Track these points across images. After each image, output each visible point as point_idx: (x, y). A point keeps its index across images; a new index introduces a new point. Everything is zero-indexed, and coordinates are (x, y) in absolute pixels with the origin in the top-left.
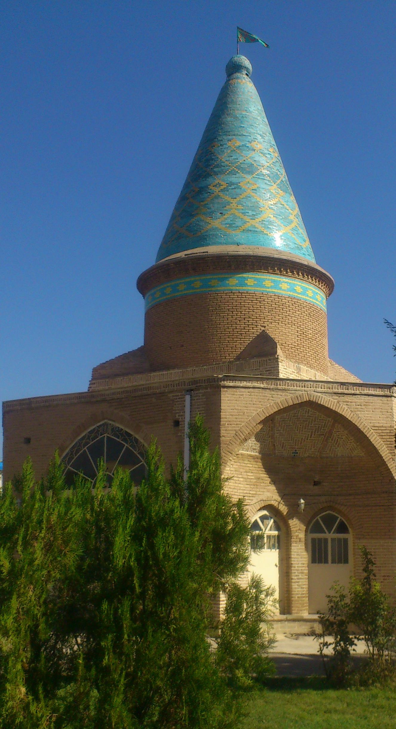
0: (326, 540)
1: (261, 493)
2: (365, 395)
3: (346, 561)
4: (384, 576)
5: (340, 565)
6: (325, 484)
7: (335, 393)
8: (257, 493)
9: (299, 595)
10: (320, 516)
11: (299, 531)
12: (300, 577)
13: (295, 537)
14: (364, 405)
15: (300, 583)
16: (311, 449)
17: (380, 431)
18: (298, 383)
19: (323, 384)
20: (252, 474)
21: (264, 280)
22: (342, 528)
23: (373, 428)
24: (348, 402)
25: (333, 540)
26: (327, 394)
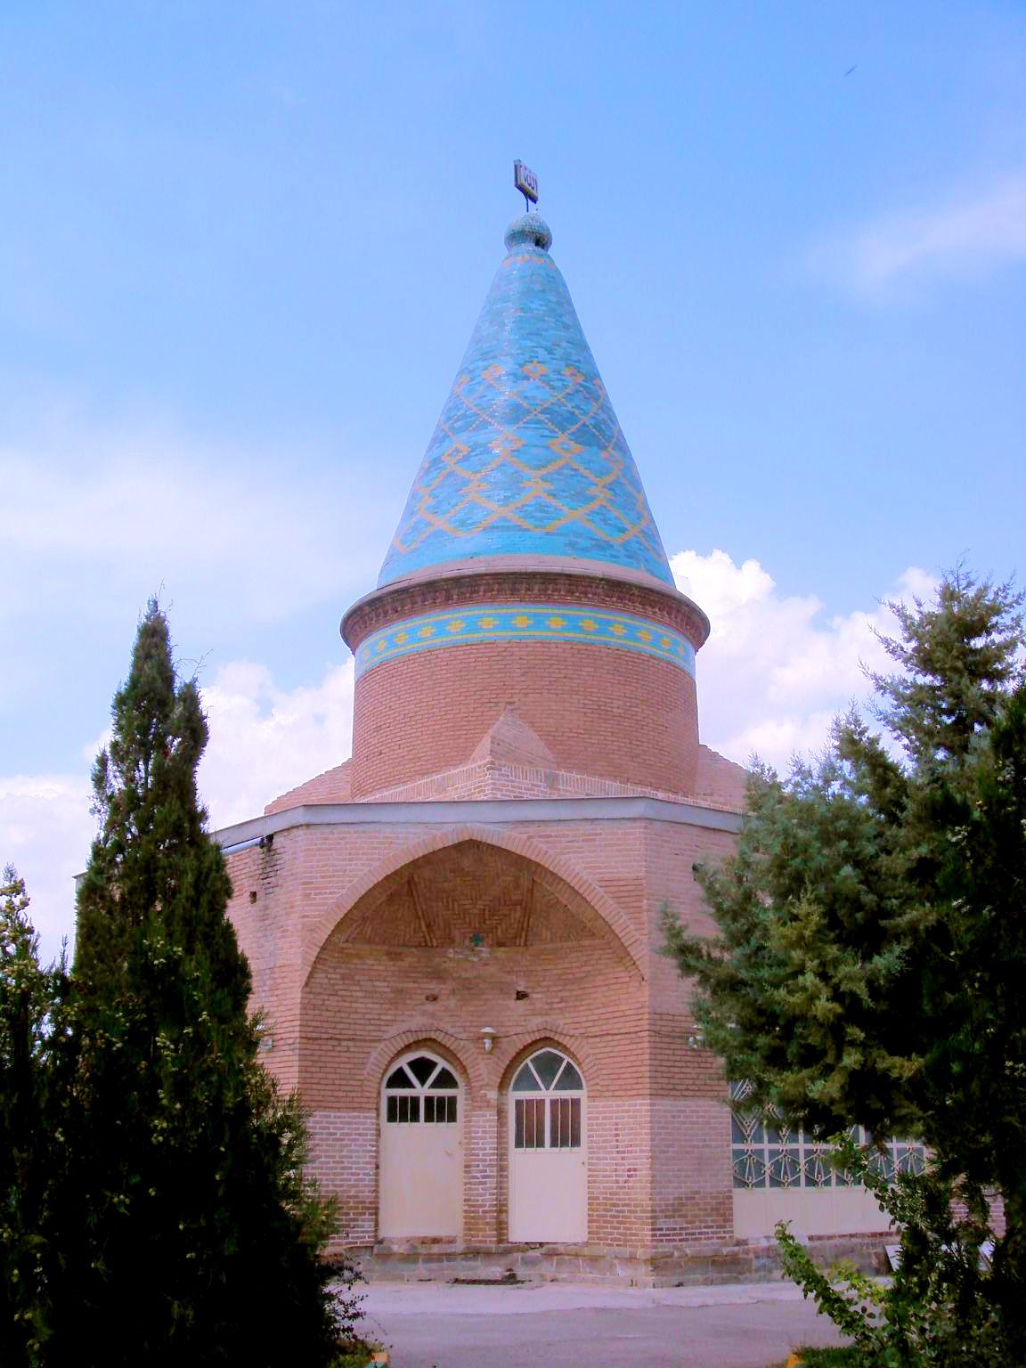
0: (541, 1102)
3: (576, 1142)
4: (629, 1170)
5: (565, 1149)
6: (535, 996)
9: (486, 1208)
10: (532, 1057)
13: (479, 1099)
14: (583, 841)
15: (488, 1185)
17: (616, 889)
22: (571, 1079)
25: (554, 1103)
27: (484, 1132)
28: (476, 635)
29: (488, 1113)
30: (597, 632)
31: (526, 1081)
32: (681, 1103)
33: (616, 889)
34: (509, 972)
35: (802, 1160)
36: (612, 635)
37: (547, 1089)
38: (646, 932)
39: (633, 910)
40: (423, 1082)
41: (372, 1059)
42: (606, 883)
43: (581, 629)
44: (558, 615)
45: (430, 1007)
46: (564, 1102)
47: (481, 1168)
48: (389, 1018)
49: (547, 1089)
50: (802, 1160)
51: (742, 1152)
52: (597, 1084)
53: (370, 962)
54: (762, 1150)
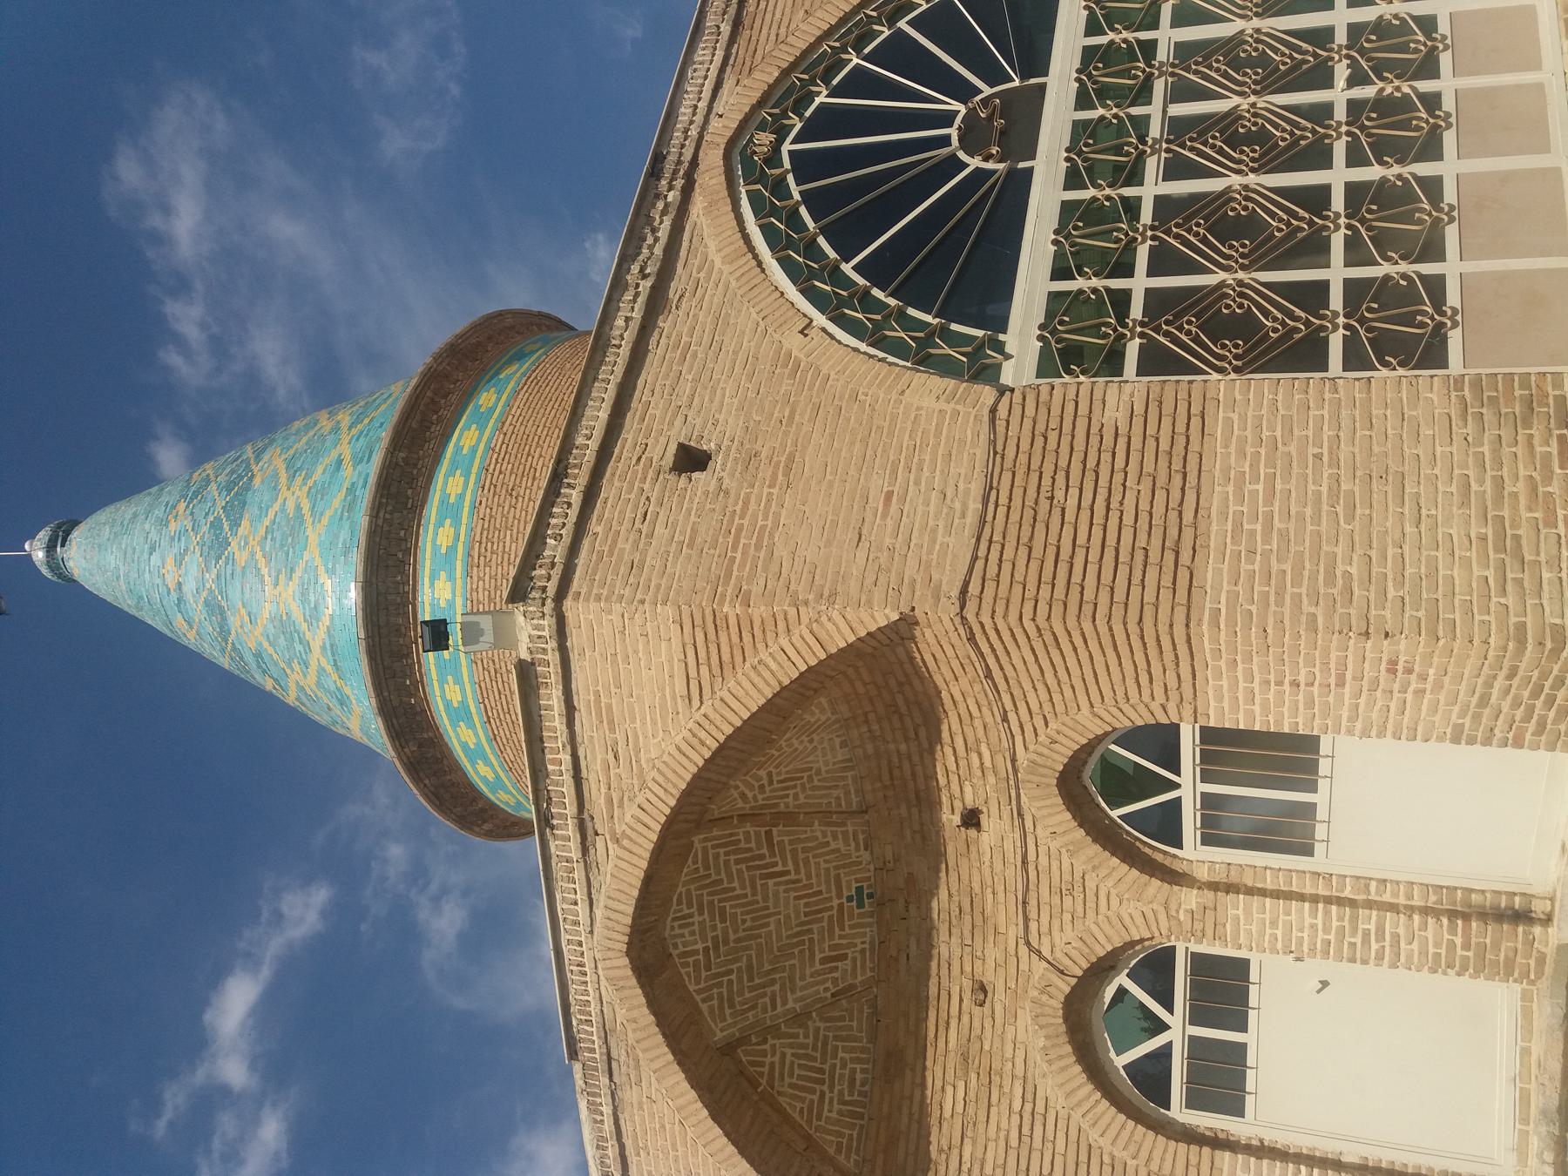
1: (1020, 1054)
2: (570, 723)
4: (1392, 671)
7: (585, 850)
8: (1019, 1071)
9: (1458, 941)
11: (1173, 907)
12: (1372, 927)
14: (612, 730)
15: (1401, 931)
16: (838, 850)
17: (704, 670)
18: (572, 988)
19: (558, 897)
20: (949, 1089)
21: (482, 428)
22: (1162, 742)
23: (696, 703)
24: (610, 801)
26: (595, 884)
27: (1274, 923)
28: (473, 710)
29: (1231, 912)
30: (456, 524)
31: (1167, 825)
32: (1216, 530)
33: (704, 670)
34: (924, 838)
35: (1373, 173)
36: (461, 496)
37: (1178, 786)
38: (792, 612)
39: (747, 637)
40: (1163, 1027)
41: (1104, 1142)
42: (694, 692)
43: (452, 549)
44: (432, 585)
45: (999, 998)
46: (1206, 757)
47: (1358, 940)
48: (1018, 1092)
49: (1178, 786)
50: (1373, 173)
51: (1350, 344)
52: (1164, 707)
53: (905, 1120)
54: (1348, 283)
